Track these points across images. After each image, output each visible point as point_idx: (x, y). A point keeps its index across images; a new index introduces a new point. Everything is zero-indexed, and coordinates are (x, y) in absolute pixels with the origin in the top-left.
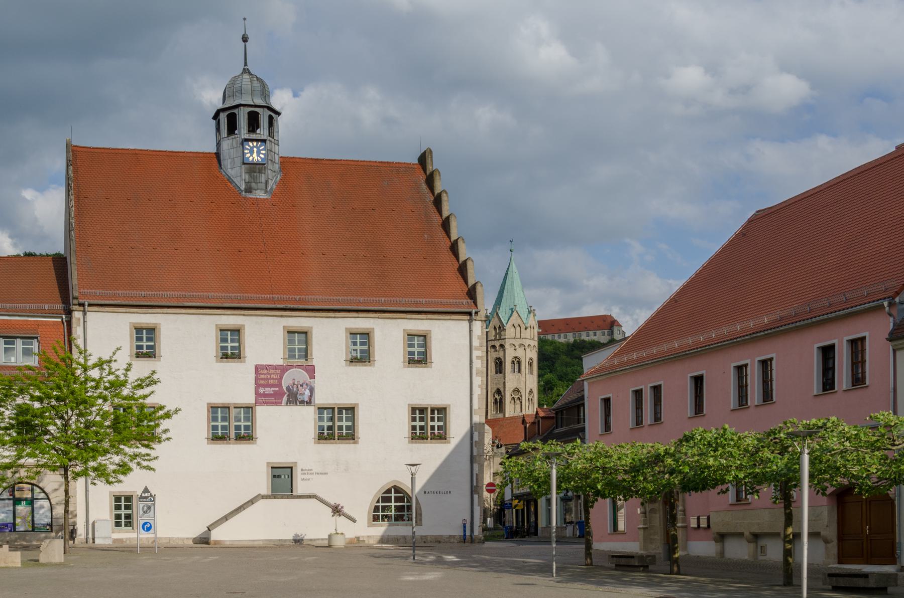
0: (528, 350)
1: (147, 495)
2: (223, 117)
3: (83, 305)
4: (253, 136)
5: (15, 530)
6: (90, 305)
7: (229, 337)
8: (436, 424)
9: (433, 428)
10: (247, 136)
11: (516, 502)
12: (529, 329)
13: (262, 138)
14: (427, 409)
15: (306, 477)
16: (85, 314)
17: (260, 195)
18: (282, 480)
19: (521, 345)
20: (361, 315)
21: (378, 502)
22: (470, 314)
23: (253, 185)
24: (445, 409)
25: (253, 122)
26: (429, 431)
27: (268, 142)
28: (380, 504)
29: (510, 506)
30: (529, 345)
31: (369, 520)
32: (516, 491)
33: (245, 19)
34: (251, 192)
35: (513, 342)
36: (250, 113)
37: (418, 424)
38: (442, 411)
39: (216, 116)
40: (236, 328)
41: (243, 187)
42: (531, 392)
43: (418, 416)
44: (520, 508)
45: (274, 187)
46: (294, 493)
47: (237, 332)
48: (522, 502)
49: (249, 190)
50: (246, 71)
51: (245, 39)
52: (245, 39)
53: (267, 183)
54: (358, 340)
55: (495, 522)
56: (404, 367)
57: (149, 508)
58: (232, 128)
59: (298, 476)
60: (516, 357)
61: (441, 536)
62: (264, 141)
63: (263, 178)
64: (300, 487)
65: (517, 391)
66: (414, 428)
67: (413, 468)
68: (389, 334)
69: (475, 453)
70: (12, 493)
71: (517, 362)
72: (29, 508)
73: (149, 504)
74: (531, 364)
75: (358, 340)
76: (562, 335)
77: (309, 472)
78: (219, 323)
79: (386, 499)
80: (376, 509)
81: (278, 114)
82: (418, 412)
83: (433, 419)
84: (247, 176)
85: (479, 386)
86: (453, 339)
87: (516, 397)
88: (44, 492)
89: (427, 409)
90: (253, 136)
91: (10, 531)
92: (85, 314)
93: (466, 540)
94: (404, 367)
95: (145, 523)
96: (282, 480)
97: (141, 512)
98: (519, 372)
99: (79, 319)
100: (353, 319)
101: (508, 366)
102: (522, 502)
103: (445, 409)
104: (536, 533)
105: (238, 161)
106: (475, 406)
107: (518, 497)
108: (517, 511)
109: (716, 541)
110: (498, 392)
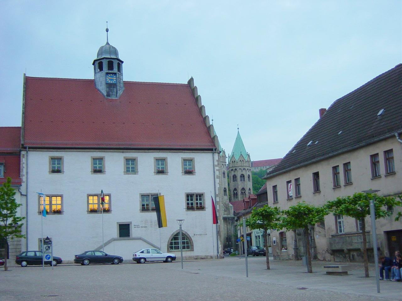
0: (247, 171)
1: (48, 241)
2: (97, 63)
3: (25, 148)
4: (110, 72)
6: (29, 148)
7: (98, 162)
8: (199, 202)
9: (197, 203)
10: (108, 72)
12: (247, 162)
13: (115, 72)
14: (194, 194)
16: (27, 152)
18: (125, 230)
19: (244, 169)
20: (161, 151)
22: (212, 150)
23: (111, 93)
24: (203, 194)
26: (196, 205)
27: (117, 74)
28: (173, 241)
30: (248, 169)
33: (107, 22)
34: (109, 96)
35: (240, 168)
36: (109, 62)
37: (190, 202)
38: (200, 196)
39: (94, 64)
40: (164, 158)
41: (105, 94)
42: (250, 189)
43: (190, 198)
47: (101, 159)
49: (108, 95)
50: (108, 43)
51: (107, 30)
52: (107, 30)
54: (160, 163)
57: (49, 247)
58: (101, 68)
60: (242, 174)
62: (115, 74)
65: (243, 189)
66: (188, 204)
68: (175, 161)
71: (242, 176)
73: (49, 245)
74: (249, 177)
76: (264, 167)
77: (137, 226)
80: (171, 243)
81: (122, 62)
82: (189, 196)
83: (197, 200)
84: (108, 89)
86: (203, 162)
87: (243, 192)
89: (194, 194)
90: (110, 72)
92: (27, 152)
93: (218, 257)
94: (182, 175)
95: (47, 255)
97: (45, 250)
98: (244, 181)
99: (24, 155)
100: (157, 153)
101: (239, 178)
103: (203, 194)
105: (104, 83)
106: (217, 193)
109: (331, 255)
110: (235, 189)
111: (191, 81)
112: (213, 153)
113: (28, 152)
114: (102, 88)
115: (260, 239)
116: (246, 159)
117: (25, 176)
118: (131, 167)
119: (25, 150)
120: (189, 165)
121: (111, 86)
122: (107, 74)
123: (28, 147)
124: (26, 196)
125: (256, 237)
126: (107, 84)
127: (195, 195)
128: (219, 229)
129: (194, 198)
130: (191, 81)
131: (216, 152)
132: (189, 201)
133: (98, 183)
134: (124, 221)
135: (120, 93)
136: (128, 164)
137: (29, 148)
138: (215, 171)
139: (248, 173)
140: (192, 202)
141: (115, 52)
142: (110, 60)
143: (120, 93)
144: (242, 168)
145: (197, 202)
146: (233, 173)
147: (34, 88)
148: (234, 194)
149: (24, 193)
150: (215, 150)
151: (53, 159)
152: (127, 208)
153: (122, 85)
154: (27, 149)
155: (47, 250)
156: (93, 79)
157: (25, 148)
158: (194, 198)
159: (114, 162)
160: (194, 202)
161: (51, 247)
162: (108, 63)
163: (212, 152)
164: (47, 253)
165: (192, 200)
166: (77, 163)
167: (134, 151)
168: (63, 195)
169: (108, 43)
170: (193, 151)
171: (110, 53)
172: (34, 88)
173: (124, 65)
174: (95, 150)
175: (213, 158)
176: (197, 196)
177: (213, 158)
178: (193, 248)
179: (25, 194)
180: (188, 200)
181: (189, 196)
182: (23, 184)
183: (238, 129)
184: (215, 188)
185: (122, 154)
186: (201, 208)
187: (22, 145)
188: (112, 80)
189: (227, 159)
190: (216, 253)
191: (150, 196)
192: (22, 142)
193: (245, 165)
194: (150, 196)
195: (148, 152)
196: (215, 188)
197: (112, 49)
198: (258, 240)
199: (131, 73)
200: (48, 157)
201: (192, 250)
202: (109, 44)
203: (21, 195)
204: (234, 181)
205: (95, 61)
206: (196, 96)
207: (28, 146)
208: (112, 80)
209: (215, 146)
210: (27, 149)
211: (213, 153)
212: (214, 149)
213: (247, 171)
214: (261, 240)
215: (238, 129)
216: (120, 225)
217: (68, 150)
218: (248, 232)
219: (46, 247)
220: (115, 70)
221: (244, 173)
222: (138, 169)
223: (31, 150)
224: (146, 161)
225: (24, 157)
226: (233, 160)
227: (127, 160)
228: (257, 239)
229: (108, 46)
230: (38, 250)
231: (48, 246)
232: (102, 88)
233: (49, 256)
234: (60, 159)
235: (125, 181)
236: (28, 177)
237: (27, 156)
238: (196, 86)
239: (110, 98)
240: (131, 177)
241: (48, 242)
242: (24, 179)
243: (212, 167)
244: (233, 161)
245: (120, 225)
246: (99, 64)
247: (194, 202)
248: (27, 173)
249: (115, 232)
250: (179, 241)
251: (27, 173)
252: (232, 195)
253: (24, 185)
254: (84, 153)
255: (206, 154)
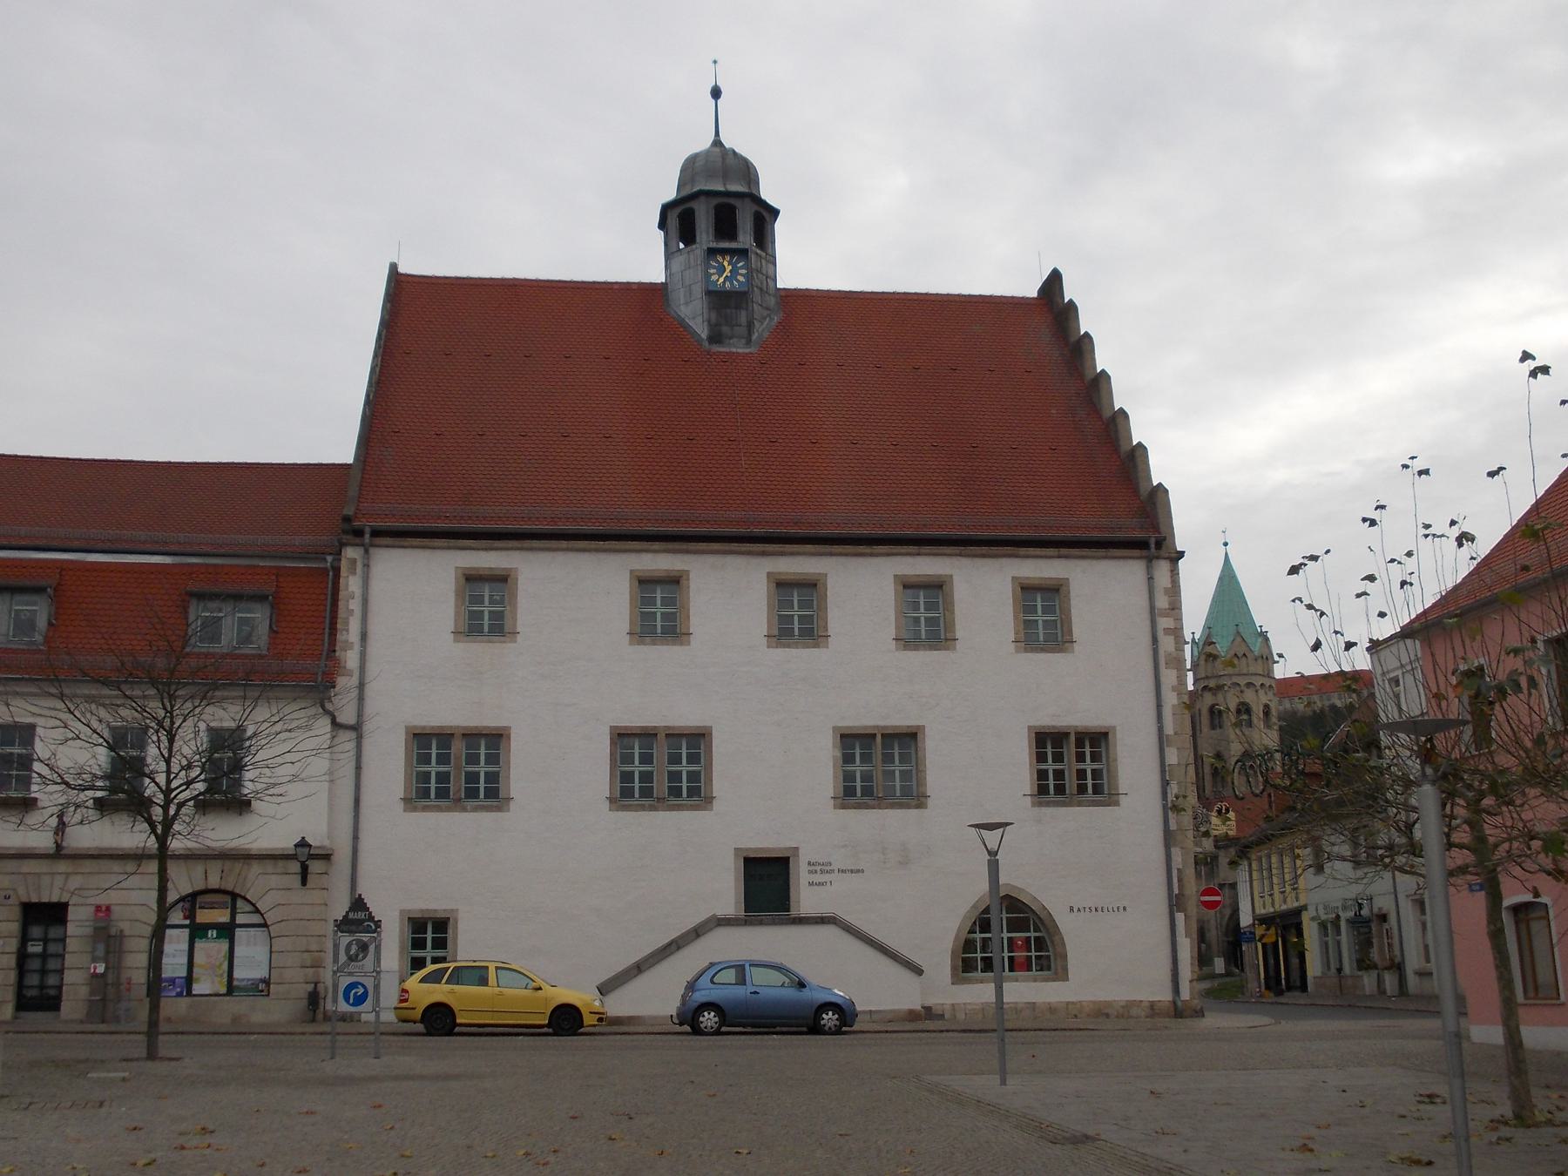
0: (1261, 692)
1: (361, 915)
2: (673, 221)
3: (359, 533)
5: (189, 993)
6: (376, 533)
8: (1089, 766)
11: (1259, 931)
15: (818, 878)
16: (367, 551)
17: (739, 348)
18: (767, 884)
19: (1249, 685)
21: (971, 931)
22: (1141, 545)
23: (725, 329)
24: (1106, 734)
25: (725, 225)
29: (1251, 937)
31: (954, 968)
32: (1260, 911)
38: (1096, 741)
44: (1269, 940)
45: (766, 334)
46: (793, 912)
47: (675, 581)
48: (1273, 930)
49: (716, 338)
50: (717, 143)
51: (716, 93)
52: (716, 93)
53: (750, 326)
54: (922, 601)
55: (1227, 963)
56: (1017, 651)
57: (364, 947)
59: (801, 877)
60: (1243, 704)
61: (1108, 1004)
62: (743, 253)
63: (743, 317)
64: (806, 899)
67: (992, 837)
68: (984, 590)
69: (1173, 826)
70: (191, 915)
71: (1244, 709)
72: (225, 946)
75: (922, 601)
78: (637, 567)
79: (983, 923)
80: (968, 945)
81: (775, 213)
82: (1047, 742)
83: (1080, 758)
84: (714, 316)
85: (1174, 689)
86: (1101, 590)
88: (257, 911)
89: (1067, 734)
91: (180, 995)
92: (367, 551)
94: (1017, 651)
96: (767, 884)
97: (343, 958)
99: (354, 561)
102: (1273, 930)
103: (1106, 734)
104: (1303, 987)
105: (698, 290)
106: (1169, 729)
107: (1265, 921)
108: (1264, 946)
111: (1054, 282)
112: (1150, 560)
113: (372, 550)
114: (693, 313)
115: (1338, 933)
116: (1257, 648)
117: (357, 648)
118: (798, 618)
119: (358, 540)
120: (1046, 610)
121: (724, 302)
122: (712, 252)
123: (368, 530)
124: (357, 728)
125: (1323, 926)
126: (709, 293)
127: (1072, 738)
128: (1181, 887)
129: (1070, 750)
130: (1054, 282)
131: (1163, 553)
132: (1046, 761)
133: (661, 691)
134: (766, 841)
135: (762, 330)
136: (785, 603)
137: (376, 533)
138: (1160, 634)
139: (1264, 699)
140: (1081, 766)
141: (746, 171)
142: (725, 200)
143: (762, 330)
144: (1242, 681)
145: (1081, 766)
146: (1208, 699)
147: (422, 314)
148: (1215, 772)
149: (347, 716)
150: (1159, 544)
151: (472, 579)
152: (776, 787)
153: (772, 301)
154: (367, 536)
155: (352, 959)
156: (662, 279)
157: (359, 533)
158: (1070, 750)
159: (728, 594)
160: (1070, 764)
161: (372, 948)
162: (720, 209)
163: (1144, 553)
164: (351, 974)
165: (1058, 758)
166: (573, 598)
167: (809, 548)
168: (508, 728)
169: (717, 143)
170: (1064, 551)
171: (726, 174)
172: (422, 314)
173: (780, 227)
174: (645, 545)
175: (1150, 579)
176: (1080, 743)
177: (1150, 579)
178: (1065, 969)
179: (352, 721)
180: (1041, 758)
181: (1047, 742)
182: (342, 682)
183: (1226, 544)
184: (1159, 706)
185: (755, 561)
186: (427, 743)
187: (347, 519)
188: (726, 275)
189: (1188, 648)
190: (1165, 996)
191: (879, 738)
192: (349, 511)
193: (1252, 669)
194: (879, 738)
195: (872, 555)
196: (1159, 706)
197: (730, 160)
198: (1329, 939)
199: (804, 260)
200: (453, 572)
201: (1062, 975)
202: (721, 145)
203: (335, 724)
204: (1213, 727)
205: (666, 209)
206: (1073, 339)
207: (367, 525)
208: (726, 275)
209: (1155, 527)
210: (367, 536)
211: (1150, 560)
212: (1152, 541)
213: (1261, 692)
214: (1344, 937)
215: (1226, 544)
216: (747, 861)
217: (536, 543)
218: (1284, 907)
219: (349, 944)
220: (745, 239)
221: (1249, 696)
222: (830, 625)
223: (378, 541)
224: (861, 590)
225: (353, 572)
226: (1209, 649)
227: (782, 585)
228: (1326, 935)
229: (717, 150)
230: (237, 974)
231: (358, 941)
232: (693, 313)
233: (361, 990)
234: (502, 579)
235: (767, 673)
236: (369, 650)
237: (367, 566)
238: (1071, 301)
239: (716, 348)
240: (799, 658)
241: (361, 922)
242: (351, 659)
243: (1146, 615)
244: (1207, 652)
245: (747, 861)
246: (678, 219)
247: (1070, 764)
248: (364, 636)
249: (727, 895)
250: (1006, 935)
251: (364, 636)
252: (1208, 778)
253: (346, 683)
254: (602, 556)
255: (1121, 562)
